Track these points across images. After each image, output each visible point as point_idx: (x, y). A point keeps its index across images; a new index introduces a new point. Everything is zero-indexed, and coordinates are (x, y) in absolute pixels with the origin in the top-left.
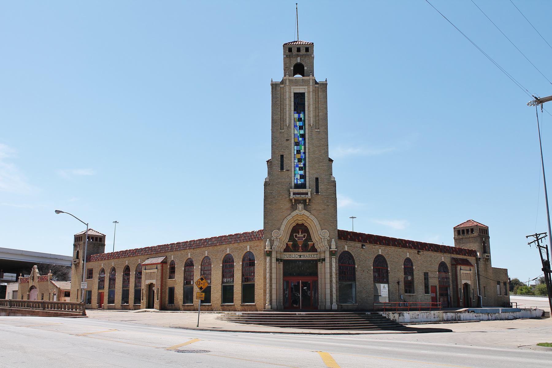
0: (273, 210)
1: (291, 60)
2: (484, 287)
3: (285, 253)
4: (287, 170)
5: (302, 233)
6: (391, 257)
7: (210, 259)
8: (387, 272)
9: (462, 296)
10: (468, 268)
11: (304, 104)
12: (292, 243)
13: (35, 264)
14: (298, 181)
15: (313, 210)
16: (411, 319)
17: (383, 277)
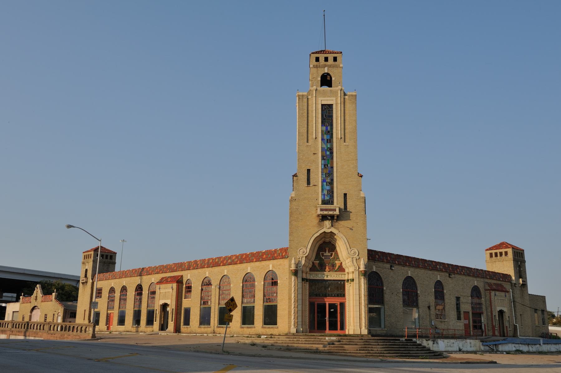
0: (299, 227)
1: (318, 70)
2: (521, 315)
3: (311, 273)
4: (314, 185)
7: (229, 278)
8: (417, 295)
9: (497, 325)
10: (503, 294)
11: (332, 116)
12: (318, 262)
13: (37, 283)
14: (326, 196)
15: (341, 227)
16: (446, 347)
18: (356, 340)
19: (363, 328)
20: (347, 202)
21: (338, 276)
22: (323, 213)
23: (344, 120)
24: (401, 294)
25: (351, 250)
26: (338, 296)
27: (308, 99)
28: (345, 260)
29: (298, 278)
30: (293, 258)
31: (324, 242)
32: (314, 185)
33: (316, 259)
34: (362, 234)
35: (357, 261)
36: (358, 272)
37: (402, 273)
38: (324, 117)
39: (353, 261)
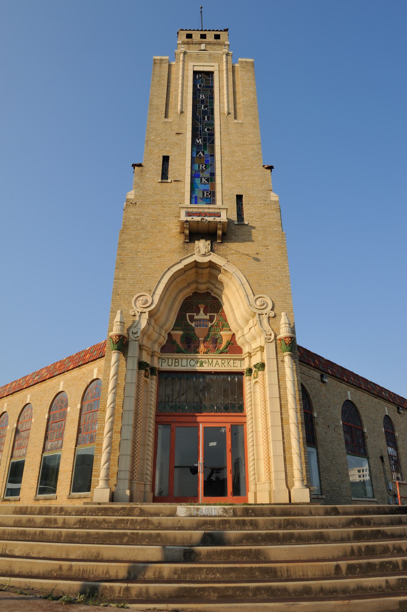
4: (175, 181)
5: (205, 312)
6: (366, 410)
12: (182, 333)
15: (232, 254)
17: (359, 443)
18: (311, 514)
19: (297, 484)
20: (243, 211)
21: (226, 364)
22: (192, 220)
23: (234, 93)
24: (342, 429)
25: (256, 297)
26: (226, 409)
27: (170, 66)
28: (243, 326)
29: (128, 358)
30: (119, 312)
31: (195, 294)
32: (175, 181)
33: (174, 328)
34: (279, 268)
35: (270, 321)
36: (273, 345)
37: (340, 392)
38: (198, 87)
39: (260, 321)
